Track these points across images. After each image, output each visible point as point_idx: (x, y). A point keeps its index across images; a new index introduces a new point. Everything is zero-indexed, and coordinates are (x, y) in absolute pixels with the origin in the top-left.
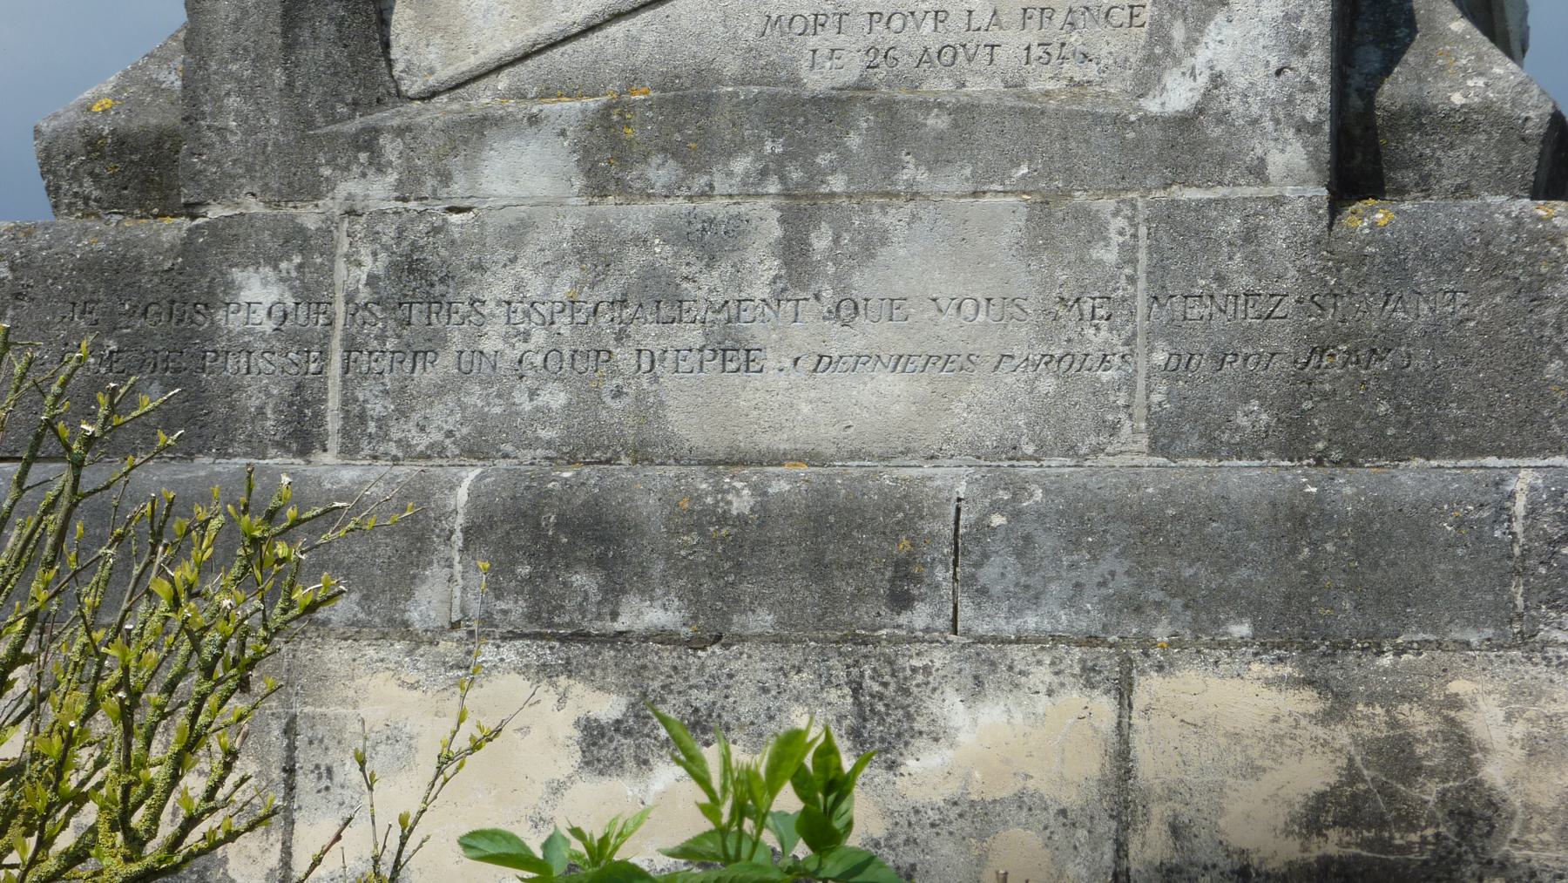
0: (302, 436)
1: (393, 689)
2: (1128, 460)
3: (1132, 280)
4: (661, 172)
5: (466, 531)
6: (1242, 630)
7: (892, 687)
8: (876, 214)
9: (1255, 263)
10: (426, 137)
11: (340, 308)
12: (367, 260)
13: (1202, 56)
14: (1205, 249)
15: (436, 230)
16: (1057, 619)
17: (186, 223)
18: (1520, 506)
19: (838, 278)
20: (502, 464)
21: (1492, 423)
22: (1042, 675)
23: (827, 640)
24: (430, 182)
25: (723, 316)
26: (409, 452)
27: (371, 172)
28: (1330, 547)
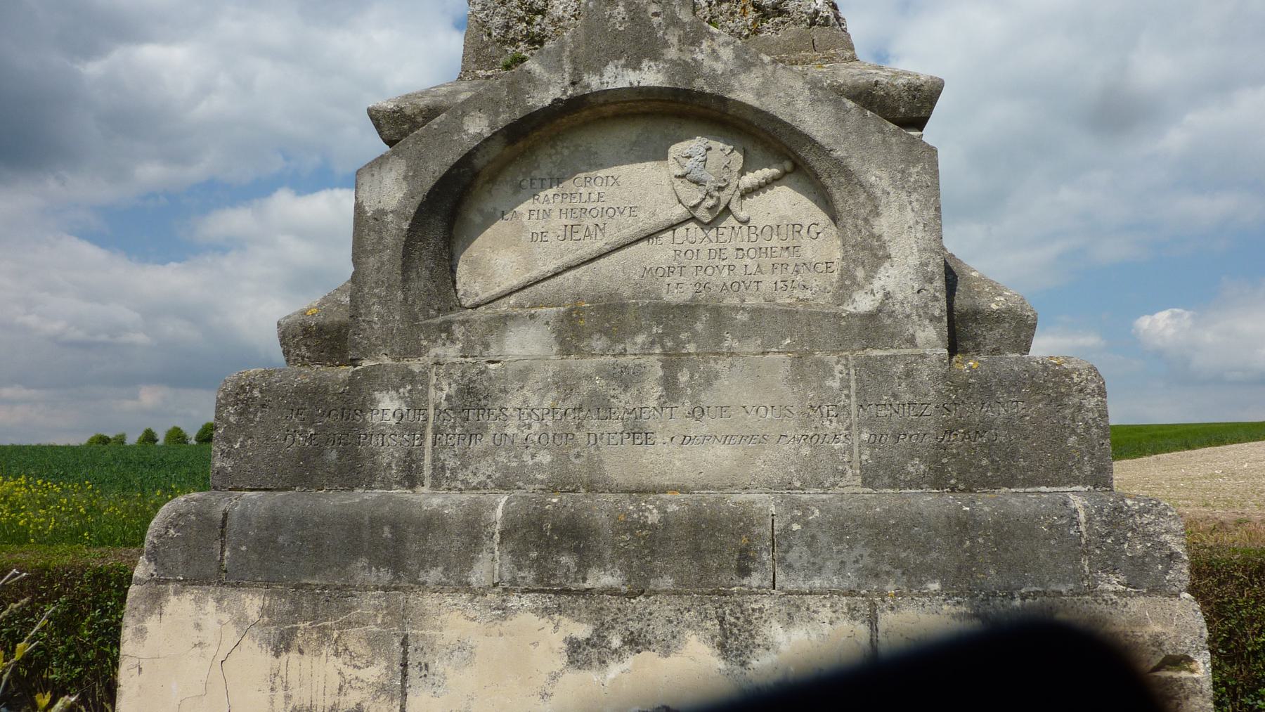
0: (411, 479)
1: (462, 620)
2: (851, 490)
3: (848, 396)
4: (598, 343)
5: (501, 533)
6: (935, 586)
7: (742, 620)
8: (712, 364)
9: (913, 388)
10: (476, 325)
11: (431, 412)
12: (446, 388)
13: (876, 284)
14: (886, 381)
15: (482, 372)
16: (832, 581)
17: (351, 369)
18: (1082, 516)
19: (693, 396)
20: (518, 493)
21: (1042, 469)
22: (826, 613)
23: (703, 593)
24: (479, 348)
25: (633, 416)
26: (468, 487)
27: (448, 343)
28: (980, 540)
